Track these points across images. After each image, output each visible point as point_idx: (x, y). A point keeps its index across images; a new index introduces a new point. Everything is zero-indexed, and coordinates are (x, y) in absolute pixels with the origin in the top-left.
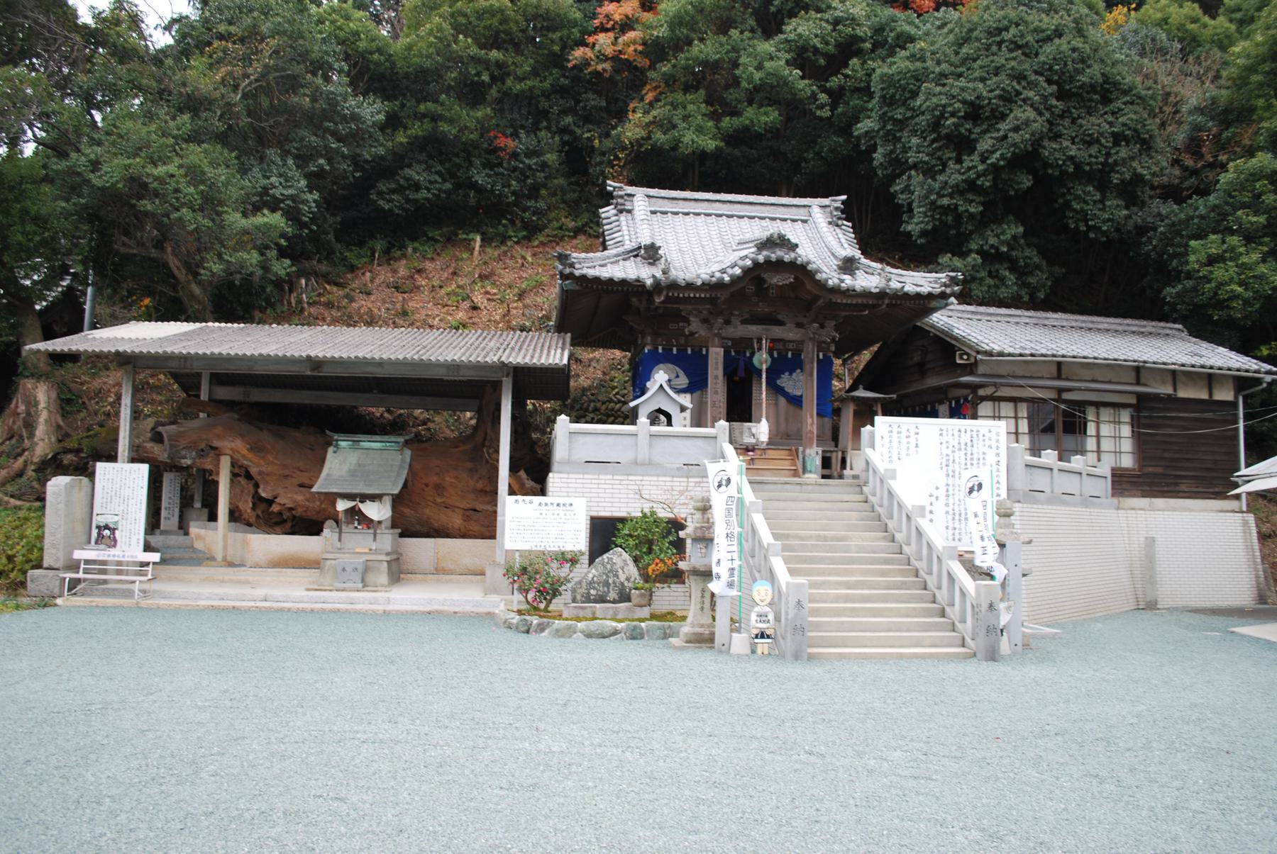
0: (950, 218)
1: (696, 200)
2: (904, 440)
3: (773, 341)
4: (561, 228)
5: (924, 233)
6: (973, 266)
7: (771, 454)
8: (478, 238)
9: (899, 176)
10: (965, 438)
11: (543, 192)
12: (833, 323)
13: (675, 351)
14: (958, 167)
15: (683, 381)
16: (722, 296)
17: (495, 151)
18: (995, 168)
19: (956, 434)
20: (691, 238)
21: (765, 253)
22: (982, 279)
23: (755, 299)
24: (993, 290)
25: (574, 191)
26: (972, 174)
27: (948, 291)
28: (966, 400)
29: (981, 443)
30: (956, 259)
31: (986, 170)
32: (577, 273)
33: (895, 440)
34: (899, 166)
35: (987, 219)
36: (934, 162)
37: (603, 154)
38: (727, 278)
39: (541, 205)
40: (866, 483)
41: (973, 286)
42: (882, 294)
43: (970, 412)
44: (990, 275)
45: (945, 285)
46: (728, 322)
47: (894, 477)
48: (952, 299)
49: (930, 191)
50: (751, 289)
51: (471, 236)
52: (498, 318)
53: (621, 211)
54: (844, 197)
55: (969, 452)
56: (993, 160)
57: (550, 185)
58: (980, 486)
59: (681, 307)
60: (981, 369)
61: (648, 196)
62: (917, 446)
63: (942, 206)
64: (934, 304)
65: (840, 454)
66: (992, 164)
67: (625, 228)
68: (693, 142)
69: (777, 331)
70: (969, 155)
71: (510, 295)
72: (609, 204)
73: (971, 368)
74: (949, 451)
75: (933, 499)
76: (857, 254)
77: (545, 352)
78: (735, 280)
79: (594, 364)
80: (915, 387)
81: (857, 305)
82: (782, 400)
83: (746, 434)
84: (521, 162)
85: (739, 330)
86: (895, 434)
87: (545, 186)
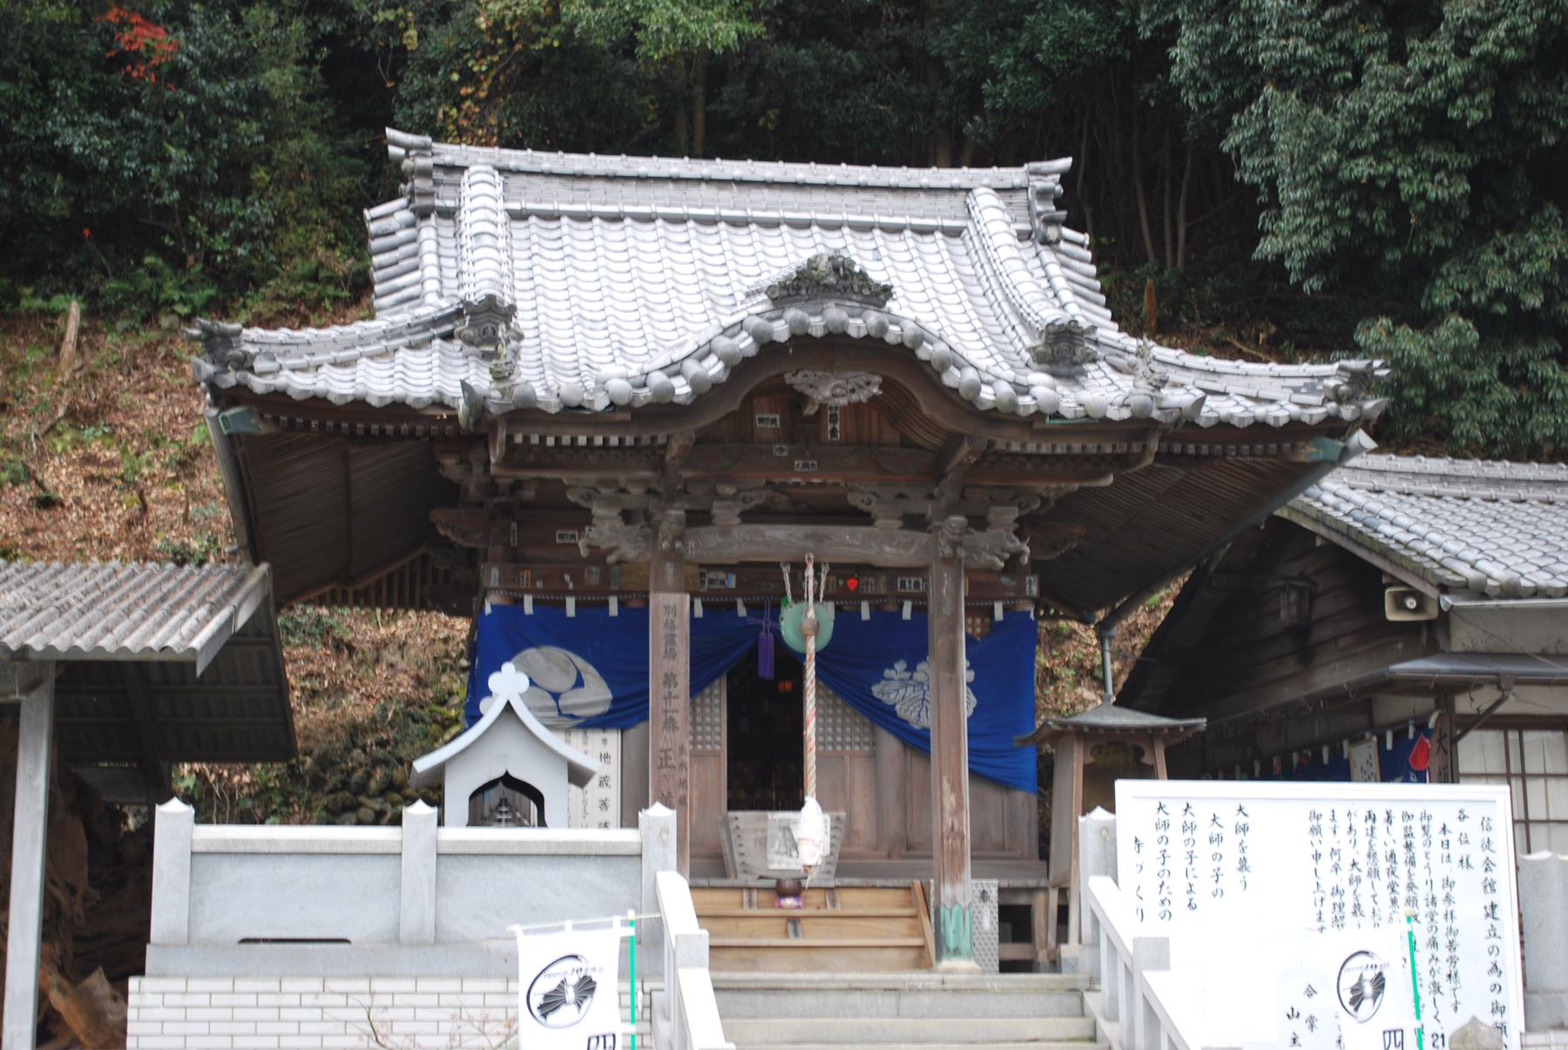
0: (1380, 215)
1: (642, 179)
2: (1204, 849)
3: (838, 569)
4: (314, 277)
5: (1316, 264)
6: (1455, 351)
7: (852, 901)
8: (75, 308)
9: (1240, 106)
10: (1390, 839)
11: (260, 174)
12: (1012, 514)
13: (571, 609)
14: (1395, 70)
15: (596, 694)
16: (678, 440)
17: (124, 59)
18: (1500, 75)
19: (1361, 826)
20: (598, 283)
21: (793, 313)
22: (1480, 388)
23: (781, 451)
24: (1514, 419)
25: (353, 171)
26: (1434, 90)
27: (1347, 412)
28: (1422, 727)
29: (1436, 851)
30: (1404, 331)
31: (1469, 77)
32: (259, 384)
33: (1177, 850)
34: (1237, 76)
35: (1490, 211)
36: (1329, 60)
37: (431, 67)
38: (682, 388)
39: (259, 210)
40: (1093, 983)
41: (1458, 410)
42: (1139, 426)
43: (1435, 763)
44: (1505, 374)
45: (1338, 397)
46: (699, 518)
47: (1161, 961)
48: (1361, 438)
49: (1320, 141)
50: (768, 420)
51: (58, 302)
52: (111, 529)
53: (423, 214)
54: (1065, 163)
55: (1403, 881)
56: (1488, 46)
57: (279, 155)
58: (1379, 983)
59: (566, 477)
60: (1462, 637)
61: (502, 171)
62: (1243, 865)
63: (1354, 184)
64: (1309, 452)
65: (1054, 896)
66: (1482, 58)
67: (429, 259)
68: (674, 26)
69: (848, 543)
70: (1426, 36)
71: (153, 464)
72: (393, 195)
73: (1430, 633)
74: (1342, 879)
75: (1299, 1026)
76: (1098, 319)
77: (158, 615)
78: (706, 394)
79: (390, 656)
80: (1290, 693)
81: (1070, 457)
82: (890, 745)
83: (776, 845)
84: (194, 91)
85: (739, 541)
86: (1175, 833)
87: (266, 159)
